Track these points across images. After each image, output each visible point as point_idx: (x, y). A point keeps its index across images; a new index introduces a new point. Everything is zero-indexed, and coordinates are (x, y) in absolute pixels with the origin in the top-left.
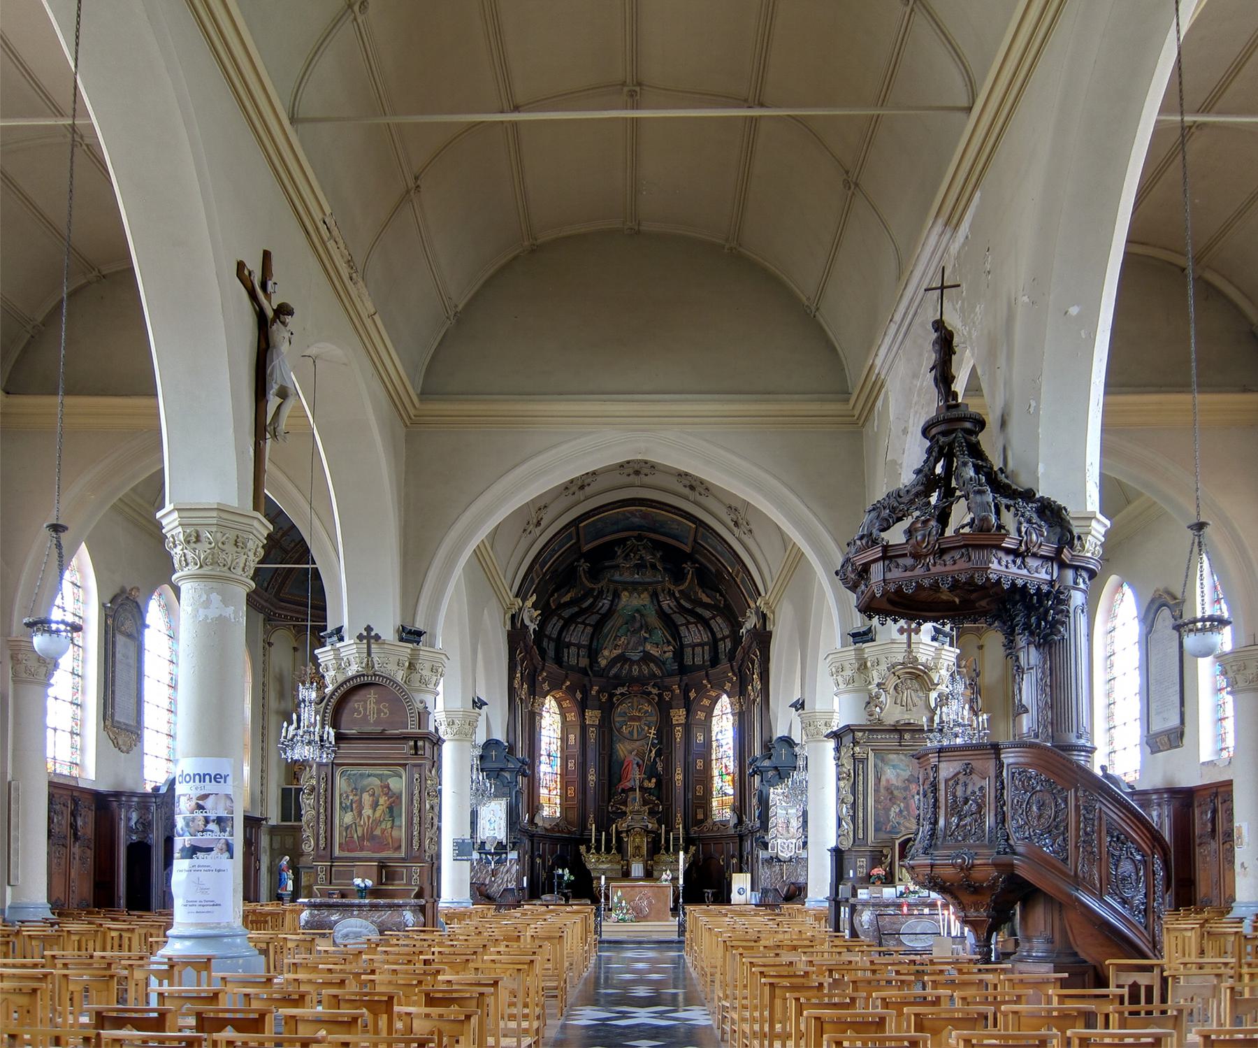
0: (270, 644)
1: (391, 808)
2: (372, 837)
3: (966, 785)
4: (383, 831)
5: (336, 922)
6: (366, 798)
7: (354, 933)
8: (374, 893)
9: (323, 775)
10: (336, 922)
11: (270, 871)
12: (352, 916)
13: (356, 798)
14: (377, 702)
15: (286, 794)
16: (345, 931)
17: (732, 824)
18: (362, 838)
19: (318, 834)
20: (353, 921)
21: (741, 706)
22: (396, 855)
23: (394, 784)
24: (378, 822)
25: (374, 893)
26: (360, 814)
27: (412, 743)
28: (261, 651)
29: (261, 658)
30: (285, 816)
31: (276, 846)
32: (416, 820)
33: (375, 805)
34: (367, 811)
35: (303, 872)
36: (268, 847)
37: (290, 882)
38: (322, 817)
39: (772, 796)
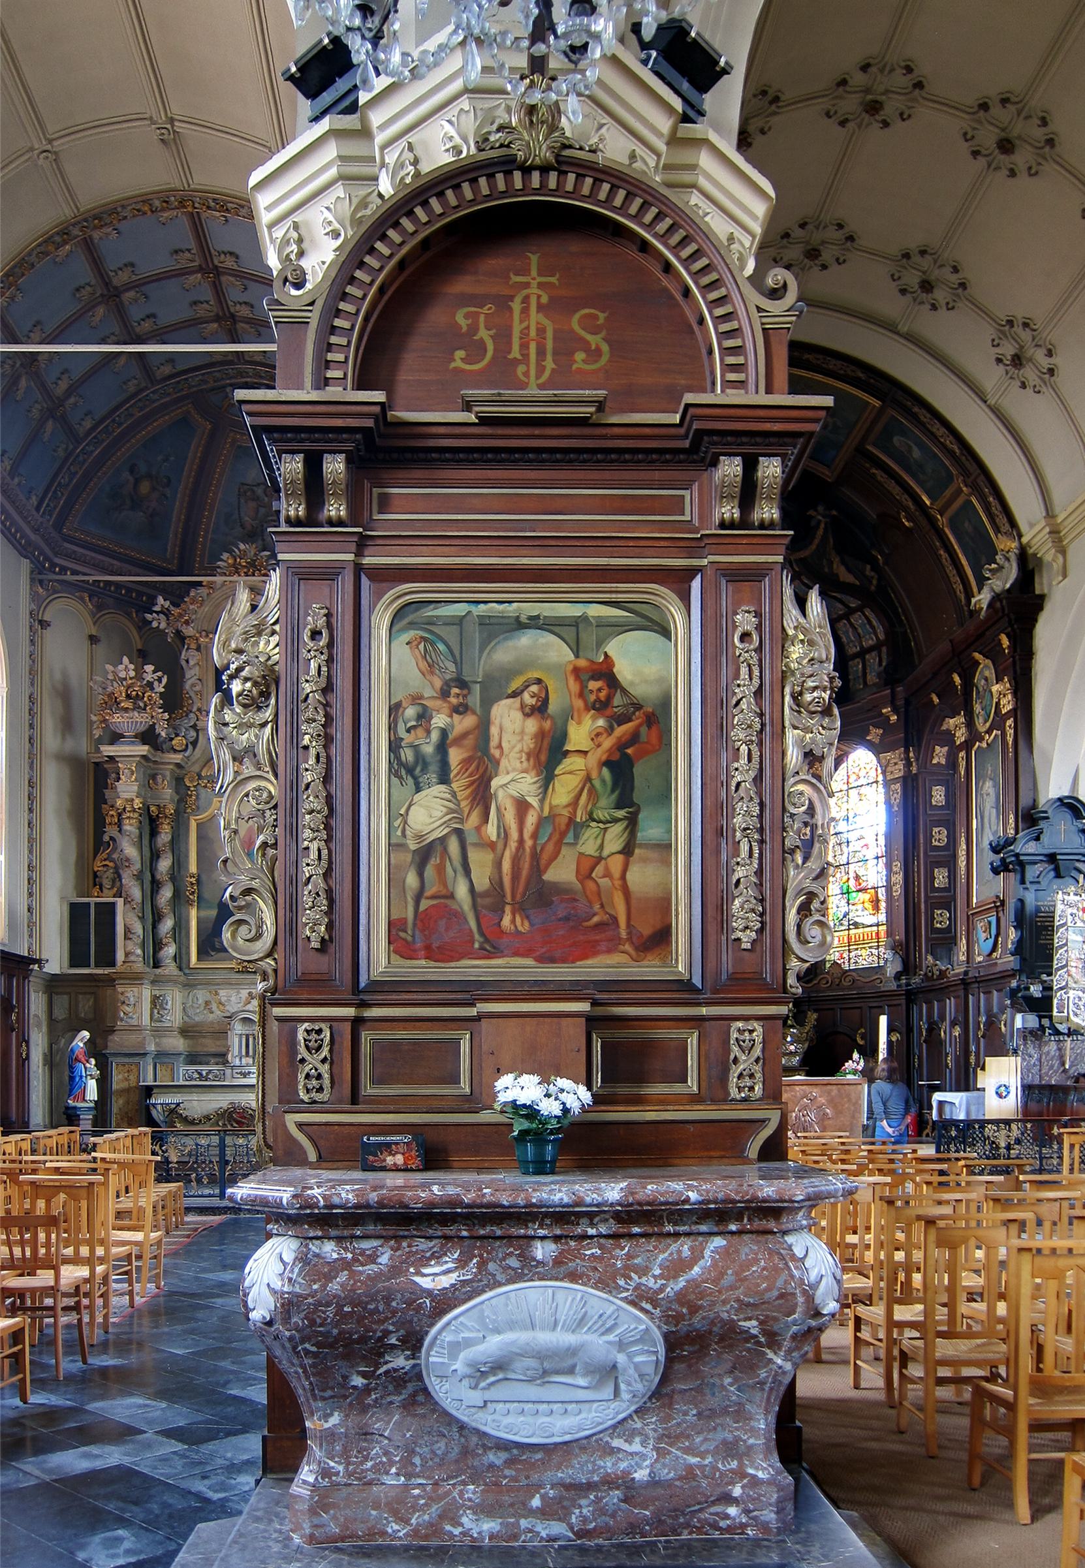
0: (44, 624)
1: (620, 768)
2: (539, 895)
3: (162, 1056)
4: (588, 867)
5: (444, 1302)
6: (511, 725)
7: (541, 1355)
8: (584, 1144)
9: (315, 619)
10: (444, 1302)
11: (50, 1061)
12: (529, 1270)
13: (468, 722)
14: (557, 306)
15: (77, 913)
16: (494, 1344)
17: (890, 971)
18: (490, 901)
19: (294, 881)
20: (533, 1295)
21: (908, 764)
22: (649, 969)
23: (634, 660)
24: (567, 828)
25: (584, 1144)
26: (482, 796)
27: (731, 468)
28: (24, 634)
29: (25, 648)
30: (77, 956)
31: (60, 1013)
32: (743, 816)
33: (549, 754)
34: (514, 781)
35: (114, 1062)
36: (43, 1017)
37: (92, 1085)
38: (312, 801)
39: (1060, 907)
